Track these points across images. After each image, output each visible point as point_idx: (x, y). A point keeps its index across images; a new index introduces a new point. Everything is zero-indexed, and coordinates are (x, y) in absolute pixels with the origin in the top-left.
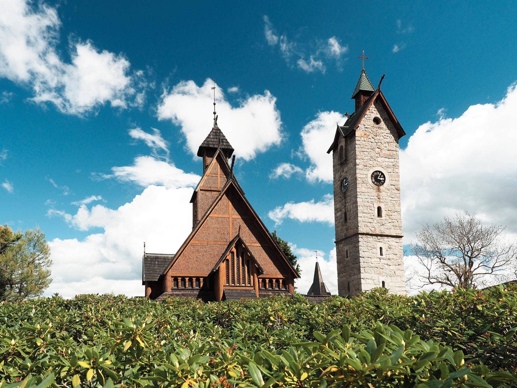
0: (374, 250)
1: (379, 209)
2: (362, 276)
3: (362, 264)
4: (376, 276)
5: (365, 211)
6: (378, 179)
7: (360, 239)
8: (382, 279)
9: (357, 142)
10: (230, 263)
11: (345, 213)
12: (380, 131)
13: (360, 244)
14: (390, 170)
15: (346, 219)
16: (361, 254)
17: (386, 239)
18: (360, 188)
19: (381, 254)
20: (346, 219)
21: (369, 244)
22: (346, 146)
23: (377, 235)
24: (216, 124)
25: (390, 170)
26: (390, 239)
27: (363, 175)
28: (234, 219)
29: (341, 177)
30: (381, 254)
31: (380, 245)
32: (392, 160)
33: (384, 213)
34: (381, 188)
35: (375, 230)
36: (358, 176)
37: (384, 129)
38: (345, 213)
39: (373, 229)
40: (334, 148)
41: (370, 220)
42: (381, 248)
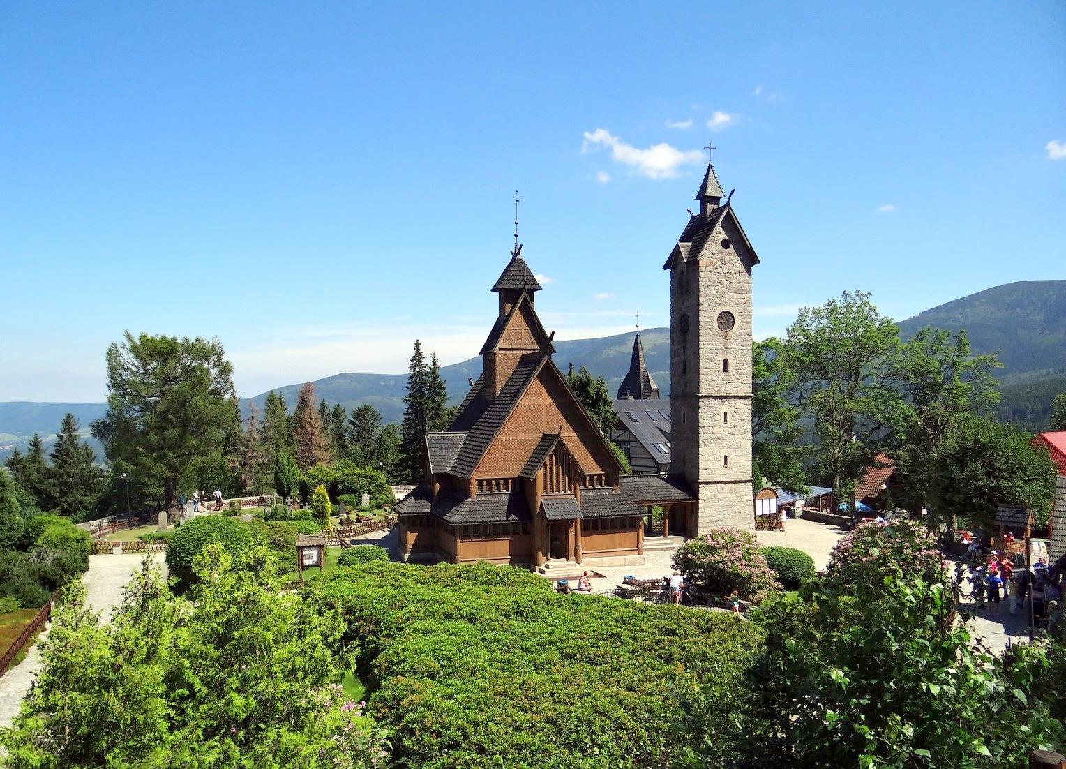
0: (718, 416)
1: (726, 362)
2: (701, 450)
3: (701, 436)
4: (716, 450)
5: (709, 365)
6: (726, 320)
7: (701, 404)
8: (724, 453)
9: (701, 274)
10: (548, 468)
11: (685, 365)
12: (728, 256)
13: (701, 410)
14: (741, 309)
15: (684, 372)
16: (702, 422)
17: (732, 401)
18: (704, 336)
19: (726, 421)
20: (684, 372)
21: (712, 409)
22: (687, 273)
23: (721, 398)
24: (519, 253)
25: (741, 309)
26: (737, 401)
27: (708, 318)
28: (549, 405)
29: (680, 309)
30: (726, 421)
31: (724, 409)
32: (744, 295)
33: (731, 367)
34: (729, 333)
35: (719, 391)
36: (701, 319)
37: (732, 257)
38: (685, 365)
39: (717, 389)
40: (673, 262)
41: (714, 378)
42: (725, 413)
